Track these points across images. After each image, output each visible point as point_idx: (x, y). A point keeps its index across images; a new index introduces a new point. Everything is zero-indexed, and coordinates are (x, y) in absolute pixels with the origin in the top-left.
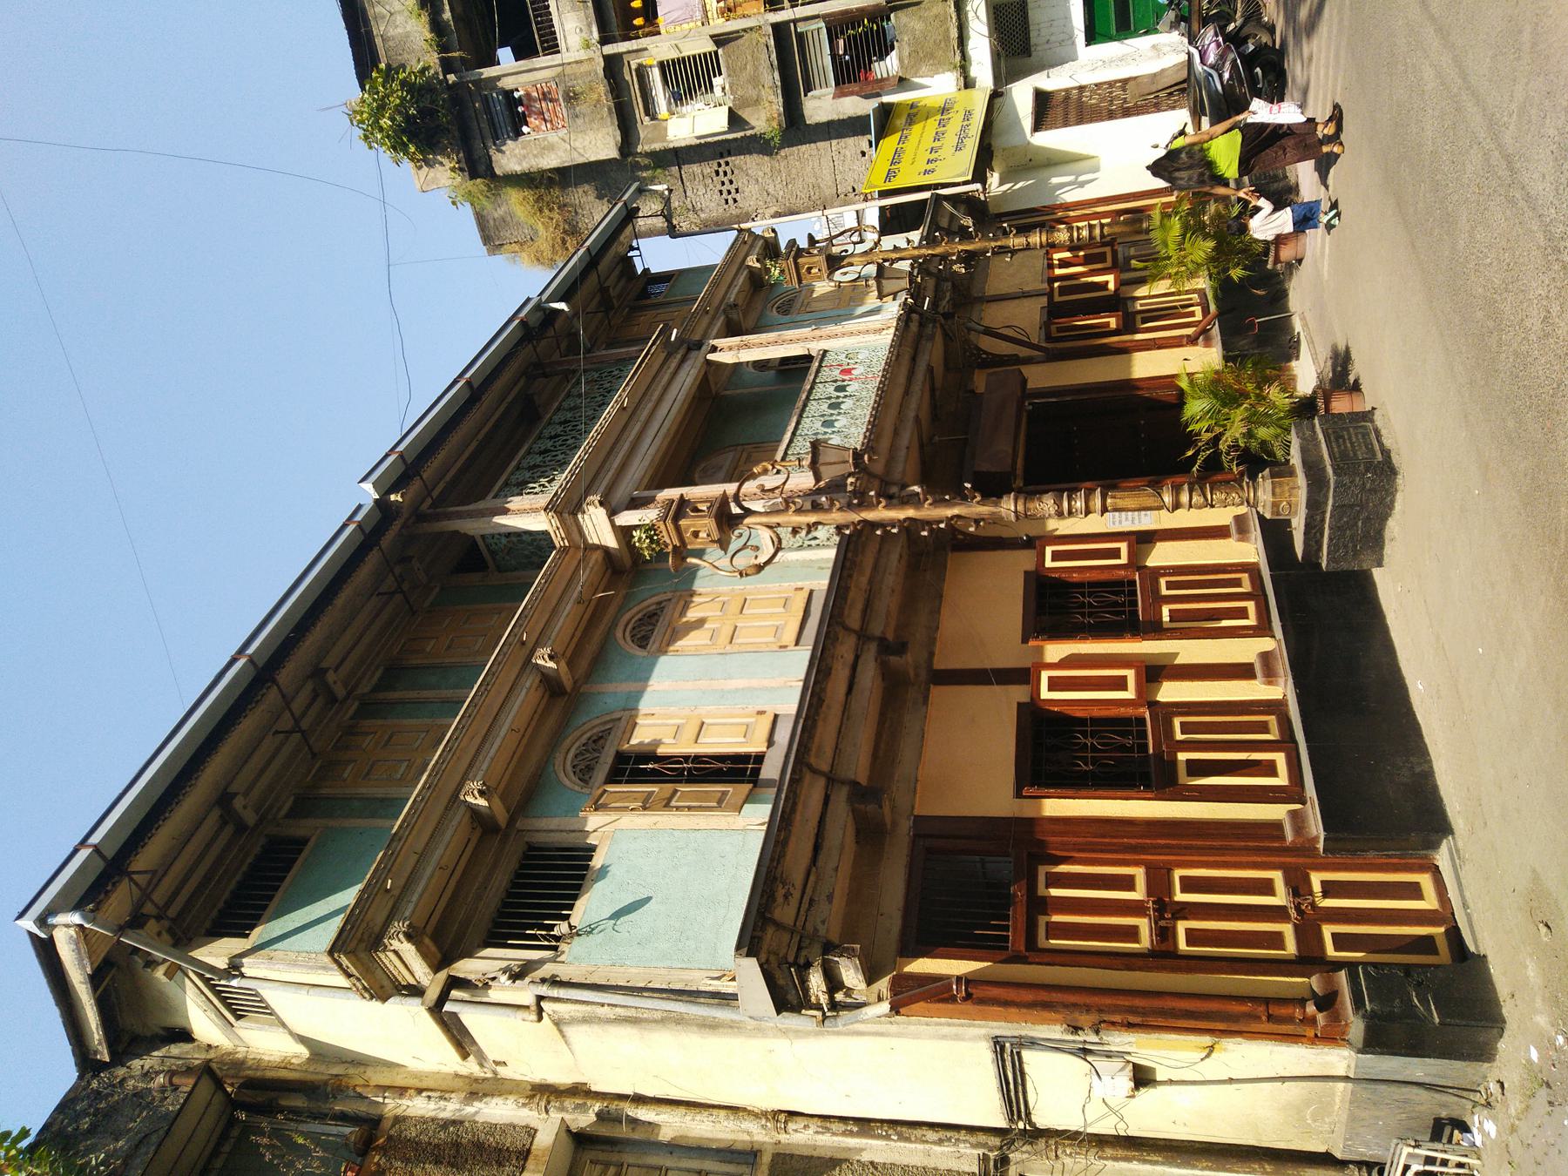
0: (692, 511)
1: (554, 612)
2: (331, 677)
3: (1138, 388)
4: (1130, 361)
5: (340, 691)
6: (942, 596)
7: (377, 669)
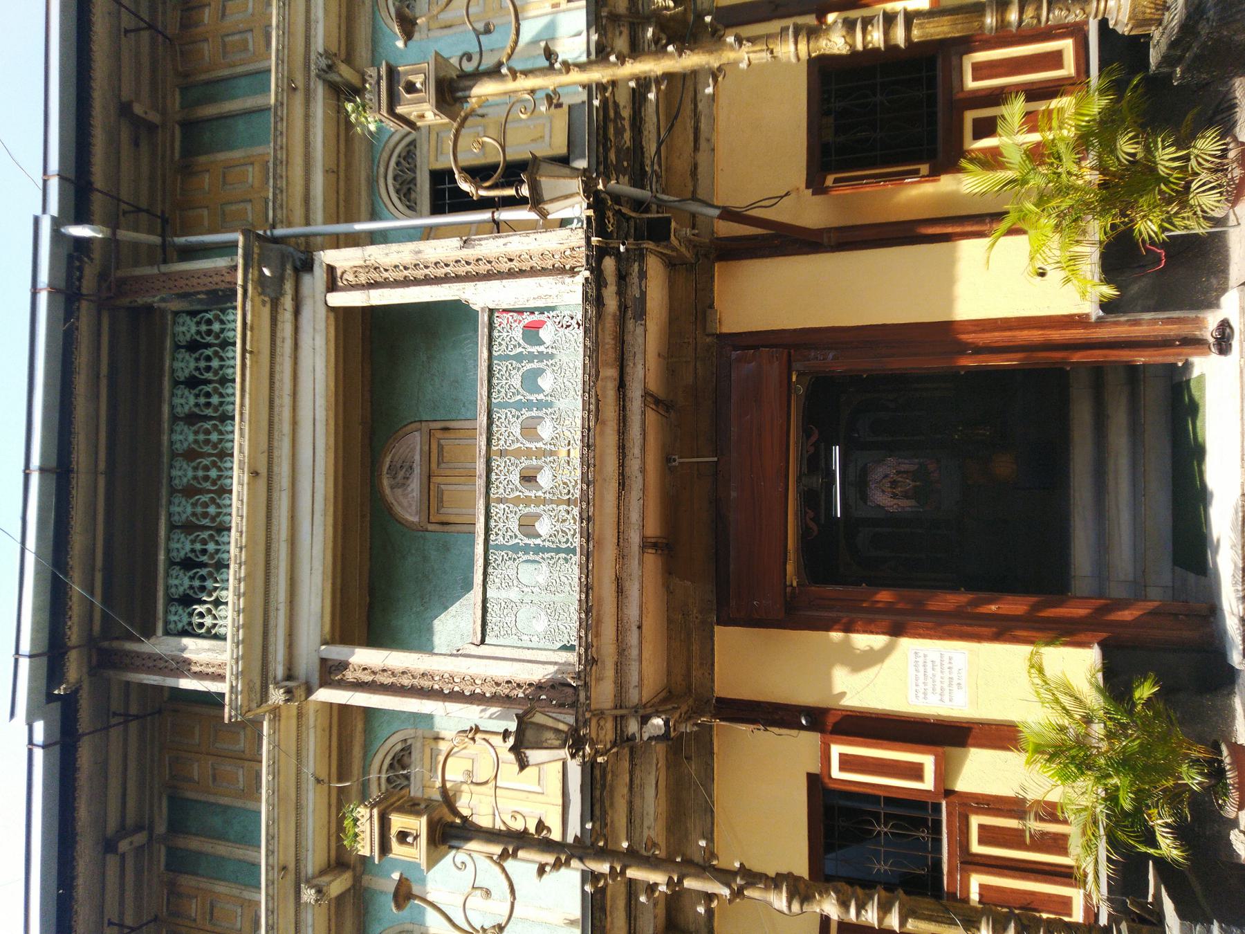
0: (409, 92)
1: (299, 807)
2: (138, 109)
3: (963, 348)
4: (953, 251)
5: (154, 117)
6: (712, 811)
7: (160, 799)
